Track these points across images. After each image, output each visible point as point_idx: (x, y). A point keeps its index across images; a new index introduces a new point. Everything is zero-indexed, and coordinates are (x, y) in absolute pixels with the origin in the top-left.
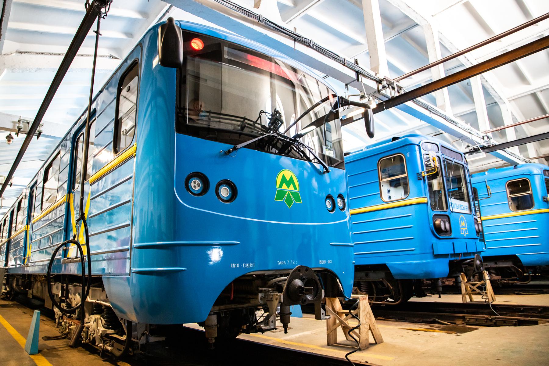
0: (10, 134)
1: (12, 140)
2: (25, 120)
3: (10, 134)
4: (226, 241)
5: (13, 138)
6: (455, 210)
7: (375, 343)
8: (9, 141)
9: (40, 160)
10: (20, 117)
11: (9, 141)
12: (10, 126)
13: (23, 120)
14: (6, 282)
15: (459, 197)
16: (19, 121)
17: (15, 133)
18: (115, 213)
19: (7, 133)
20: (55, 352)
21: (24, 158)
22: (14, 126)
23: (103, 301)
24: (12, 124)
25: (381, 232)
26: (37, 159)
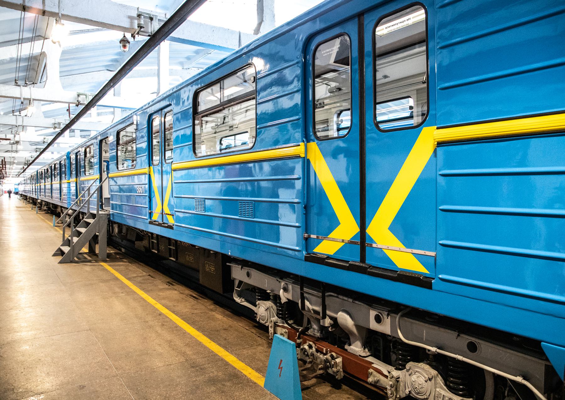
0: (124, 36)
1: (128, 45)
2: (147, 14)
3: (124, 36)
4: (230, 233)
5: (129, 43)
6: (64, 181)
7: (377, 101)
8: (124, 46)
9: (108, 70)
10: (138, 8)
11: (124, 46)
12: (126, 24)
13: (145, 13)
14: (341, 153)
15: (273, 174)
16: (139, 16)
17: (131, 34)
18: (311, 141)
19: (119, 35)
20: (350, 165)
21: (207, 92)
22: (132, 23)
23: (184, 319)
24: (128, 20)
25: (553, 342)
26: (102, 69)
